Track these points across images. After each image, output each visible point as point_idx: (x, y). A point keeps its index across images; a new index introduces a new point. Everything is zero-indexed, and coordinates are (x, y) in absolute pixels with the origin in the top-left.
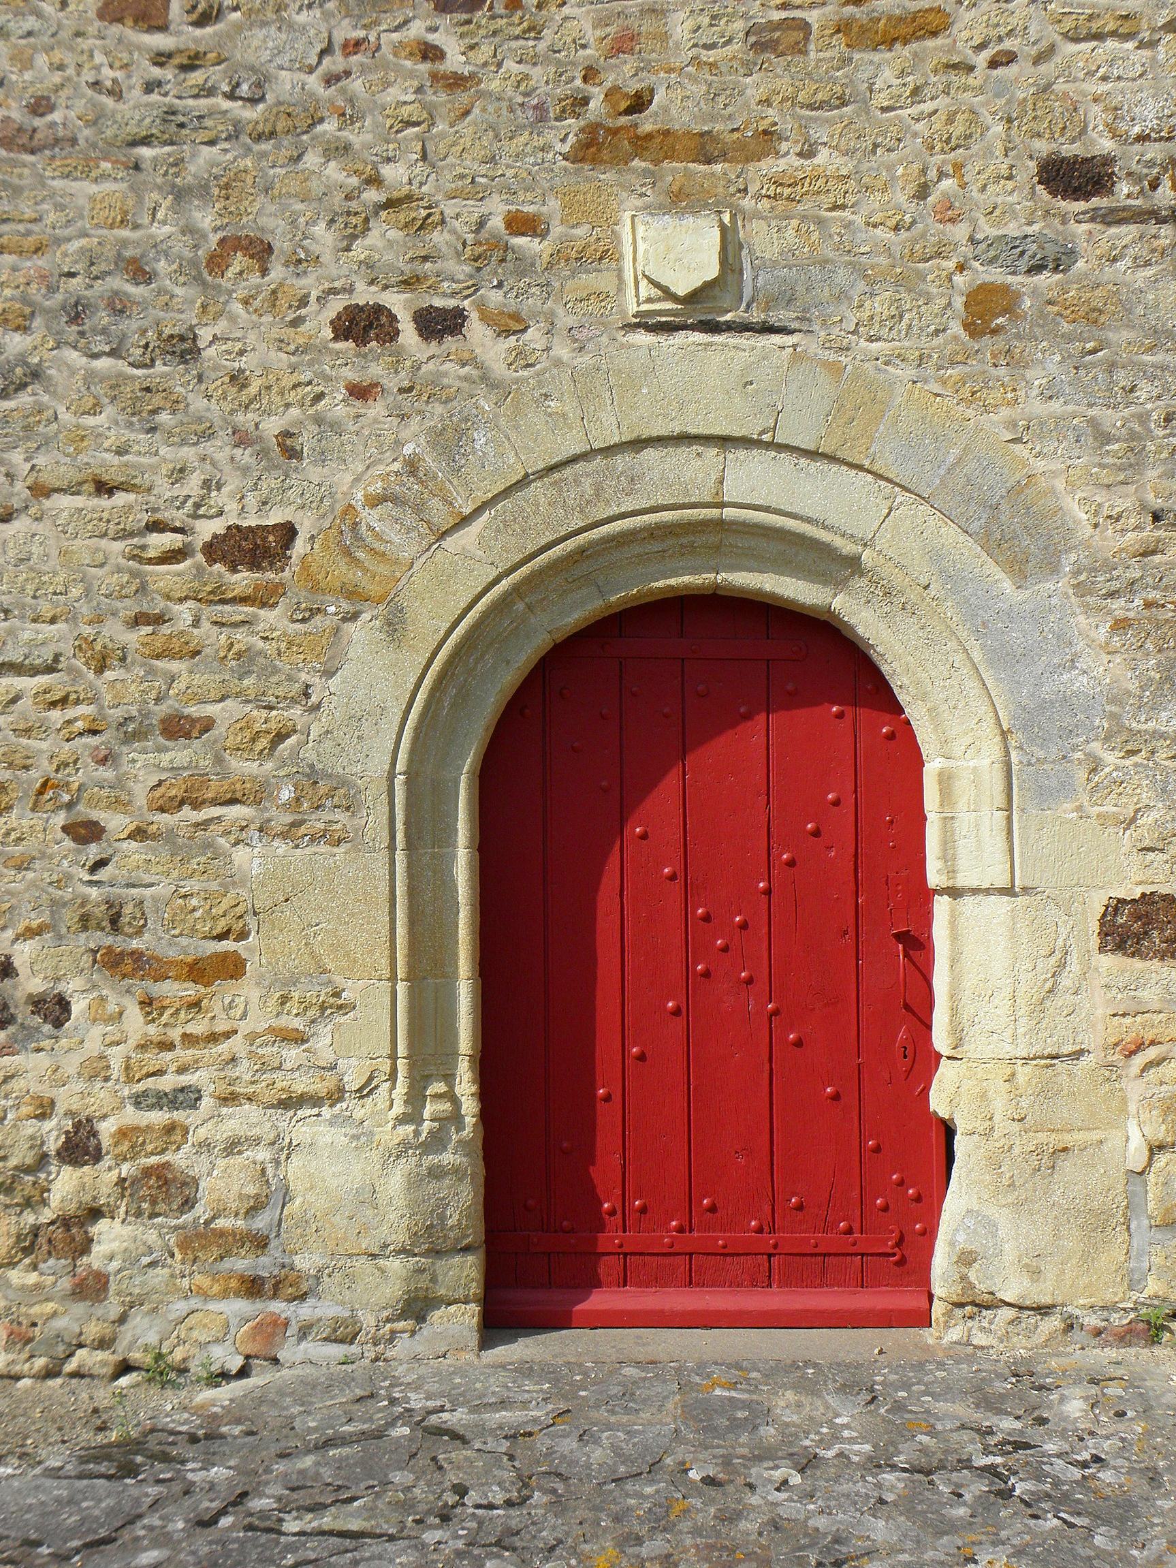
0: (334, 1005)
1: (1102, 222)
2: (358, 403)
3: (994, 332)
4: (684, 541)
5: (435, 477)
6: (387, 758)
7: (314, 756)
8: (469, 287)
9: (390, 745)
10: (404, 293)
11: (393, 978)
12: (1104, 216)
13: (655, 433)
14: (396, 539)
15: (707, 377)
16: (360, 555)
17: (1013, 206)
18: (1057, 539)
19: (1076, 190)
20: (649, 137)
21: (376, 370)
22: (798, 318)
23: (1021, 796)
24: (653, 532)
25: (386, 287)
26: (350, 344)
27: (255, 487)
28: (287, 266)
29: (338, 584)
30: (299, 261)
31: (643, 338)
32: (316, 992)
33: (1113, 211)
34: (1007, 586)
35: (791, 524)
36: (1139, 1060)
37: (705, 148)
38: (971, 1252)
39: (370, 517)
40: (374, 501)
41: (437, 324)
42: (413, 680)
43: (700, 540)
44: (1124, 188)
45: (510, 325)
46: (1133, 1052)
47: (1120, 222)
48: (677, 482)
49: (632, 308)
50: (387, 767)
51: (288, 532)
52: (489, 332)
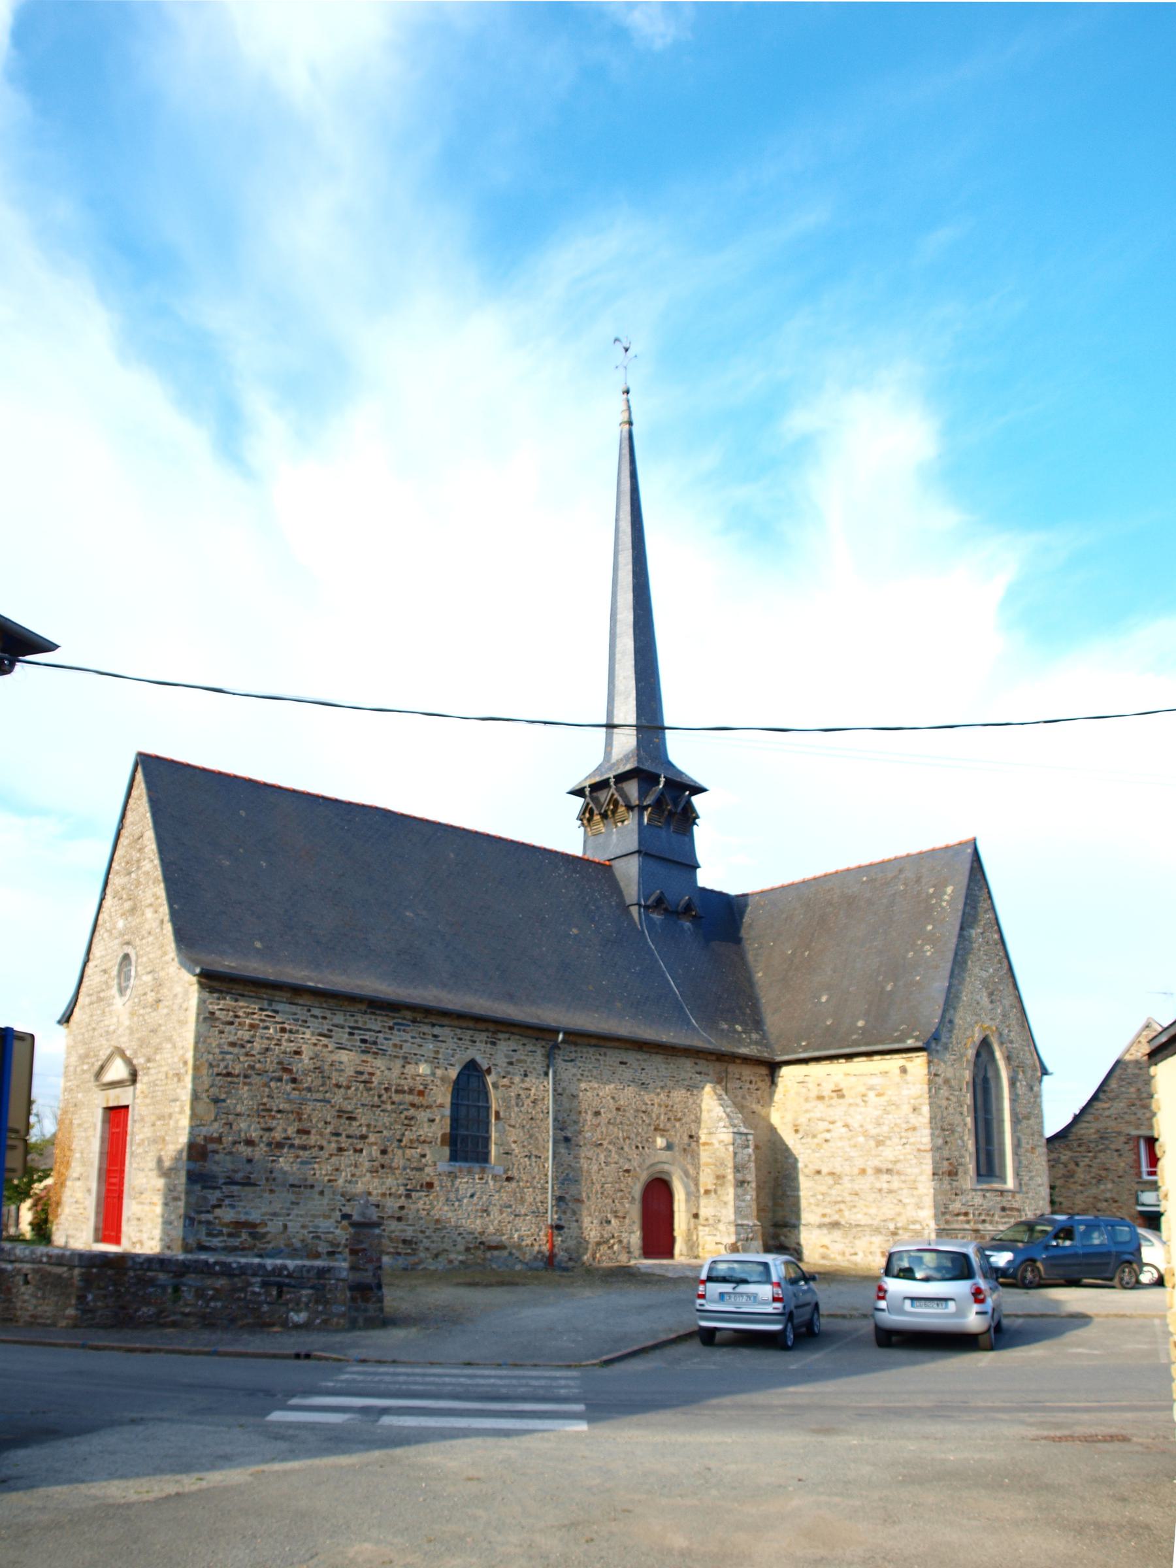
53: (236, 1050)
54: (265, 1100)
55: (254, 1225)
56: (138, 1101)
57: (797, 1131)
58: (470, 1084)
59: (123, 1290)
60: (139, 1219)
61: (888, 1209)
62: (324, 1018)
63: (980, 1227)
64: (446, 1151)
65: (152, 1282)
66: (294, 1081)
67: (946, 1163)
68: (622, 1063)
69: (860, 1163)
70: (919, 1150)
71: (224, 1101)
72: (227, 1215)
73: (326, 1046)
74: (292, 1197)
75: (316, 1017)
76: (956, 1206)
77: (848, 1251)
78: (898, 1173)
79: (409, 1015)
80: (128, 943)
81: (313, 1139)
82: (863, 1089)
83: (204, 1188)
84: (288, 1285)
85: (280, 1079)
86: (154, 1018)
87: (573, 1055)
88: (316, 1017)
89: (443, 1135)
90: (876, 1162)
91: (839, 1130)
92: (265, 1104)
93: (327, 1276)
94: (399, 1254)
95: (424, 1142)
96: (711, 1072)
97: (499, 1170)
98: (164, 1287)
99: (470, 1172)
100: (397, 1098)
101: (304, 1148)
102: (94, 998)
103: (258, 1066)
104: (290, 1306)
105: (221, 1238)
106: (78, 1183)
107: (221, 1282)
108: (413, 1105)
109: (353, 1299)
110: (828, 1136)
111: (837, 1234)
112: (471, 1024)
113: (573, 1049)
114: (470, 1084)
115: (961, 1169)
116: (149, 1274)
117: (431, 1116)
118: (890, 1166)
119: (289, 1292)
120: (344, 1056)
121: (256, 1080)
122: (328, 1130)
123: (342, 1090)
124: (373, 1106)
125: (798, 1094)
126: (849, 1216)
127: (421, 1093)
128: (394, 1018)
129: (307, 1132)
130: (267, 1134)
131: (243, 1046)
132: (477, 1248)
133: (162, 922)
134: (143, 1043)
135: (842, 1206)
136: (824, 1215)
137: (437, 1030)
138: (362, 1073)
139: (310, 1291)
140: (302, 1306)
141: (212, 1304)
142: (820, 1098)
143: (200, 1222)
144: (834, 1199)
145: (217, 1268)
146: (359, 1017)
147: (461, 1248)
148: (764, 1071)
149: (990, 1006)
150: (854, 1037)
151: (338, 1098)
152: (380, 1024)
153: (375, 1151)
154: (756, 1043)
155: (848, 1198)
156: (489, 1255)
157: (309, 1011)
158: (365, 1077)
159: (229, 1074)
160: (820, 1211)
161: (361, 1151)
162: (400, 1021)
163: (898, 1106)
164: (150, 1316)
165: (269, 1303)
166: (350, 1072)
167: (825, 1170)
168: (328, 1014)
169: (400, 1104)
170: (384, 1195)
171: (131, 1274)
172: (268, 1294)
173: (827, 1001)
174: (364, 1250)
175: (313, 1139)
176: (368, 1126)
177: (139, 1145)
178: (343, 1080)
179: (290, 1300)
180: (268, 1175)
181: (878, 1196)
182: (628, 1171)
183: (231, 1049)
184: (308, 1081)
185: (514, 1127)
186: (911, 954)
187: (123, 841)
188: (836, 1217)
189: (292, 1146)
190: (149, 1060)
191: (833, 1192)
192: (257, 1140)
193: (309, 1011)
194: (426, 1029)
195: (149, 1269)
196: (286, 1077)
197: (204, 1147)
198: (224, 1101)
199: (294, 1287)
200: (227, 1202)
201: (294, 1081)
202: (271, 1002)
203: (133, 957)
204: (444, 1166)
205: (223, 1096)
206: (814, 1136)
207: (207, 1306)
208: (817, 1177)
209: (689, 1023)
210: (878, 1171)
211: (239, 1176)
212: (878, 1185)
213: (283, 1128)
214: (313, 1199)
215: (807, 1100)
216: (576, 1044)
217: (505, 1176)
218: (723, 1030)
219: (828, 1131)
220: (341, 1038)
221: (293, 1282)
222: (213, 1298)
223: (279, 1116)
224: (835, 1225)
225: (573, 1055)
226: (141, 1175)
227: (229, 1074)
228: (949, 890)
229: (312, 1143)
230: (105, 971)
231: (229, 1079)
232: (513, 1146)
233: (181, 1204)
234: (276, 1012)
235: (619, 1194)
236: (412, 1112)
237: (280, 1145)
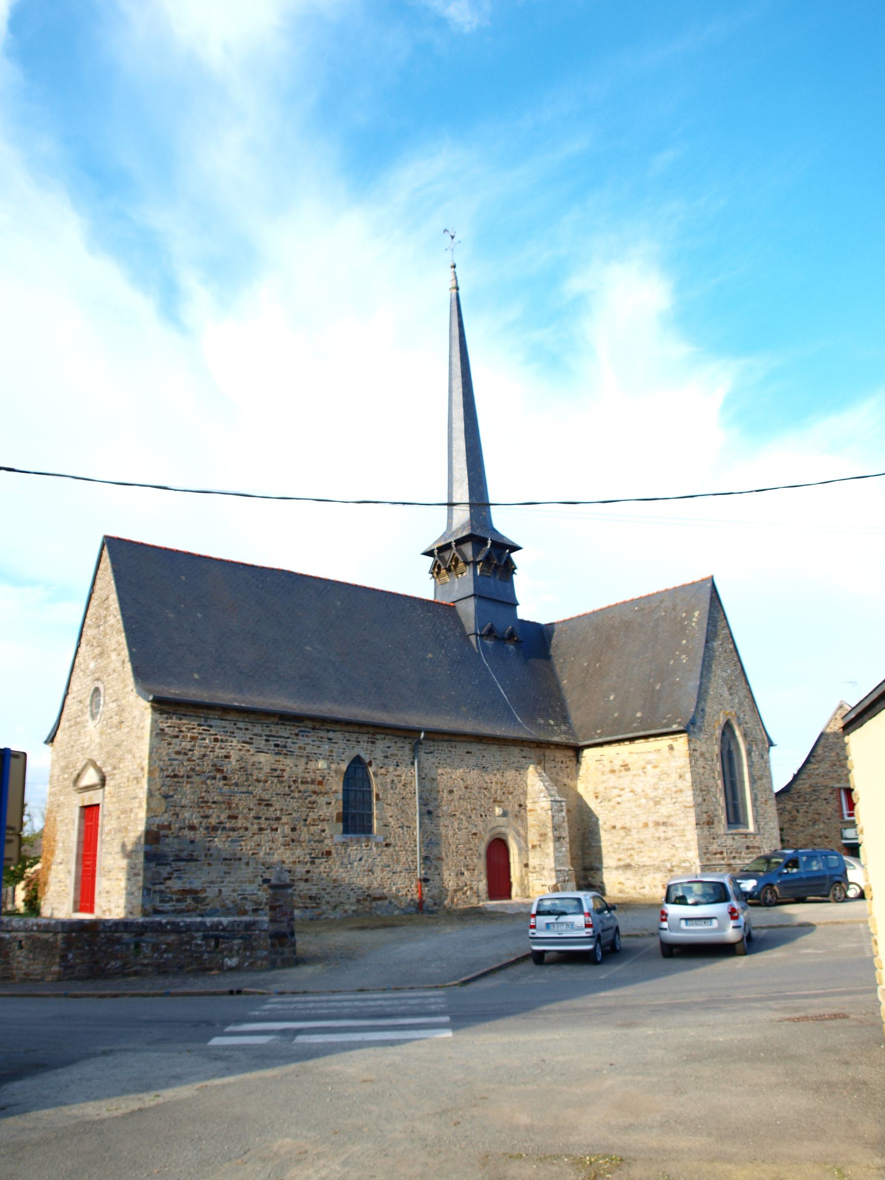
17: (517, 807)
53: (180, 757)
54: (203, 794)
55: (196, 892)
56: (106, 800)
57: (597, 797)
58: (357, 774)
59: (96, 948)
60: (108, 892)
61: (665, 852)
62: (247, 729)
63: (732, 862)
64: (340, 826)
65: (119, 941)
66: (225, 778)
67: (705, 815)
68: (468, 753)
69: (643, 819)
70: (685, 807)
71: (172, 796)
72: (176, 885)
73: (249, 751)
74: (225, 868)
75: (240, 729)
76: (714, 847)
77: (638, 886)
78: (672, 825)
79: (310, 724)
80: (98, 679)
81: (240, 822)
82: (642, 763)
83: (158, 865)
84: (223, 937)
85: (214, 778)
86: (119, 735)
87: (432, 749)
88: (240, 729)
89: (338, 814)
90: (655, 818)
91: (627, 795)
92: (203, 798)
93: (253, 928)
94: (306, 908)
95: (324, 820)
96: (533, 756)
97: (380, 839)
98: (128, 945)
99: (358, 841)
100: (302, 787)
101: (233, 829)
102: (72, 722)
103: (197, 768)
104: (225, 953)
105: (171, 904)
106: (61, 867)
107: (172, 938)
108: (315, 792)
109: (273, 945)
110: (619, 799)
111: (629, 873)
112: (356, 729)
113: (432, 743)
114: (357, 774)
115: (716, 820)
116: (117, 935)
117: (329, 800)
118: (665, 820)
119: (224, 943)
120: (262, 758)
121: (196, 779)
122: (251, 815)
123: (261, 784)
124: (284, 795)
125: (596, 769)
126: (638, 859)
127: (320, 783)
128: (299, 727)
129: (236, 818)
130: (205, 821)
131: (186, 754)
132: (365, 900)
133: (124, 662)
134: (110, 755)
135: (632, 852)
136: (619, 860)
137: (331, 735)
138: (275, 770)
139: (240, 941)
140: (234, 953)
141: (165, 956)
142: (613, 771)
143: (155, 892)
144: (626, 847)
145: (169, 927)
146: (273, 727)
147: (353, 900)
148: (571, 753)
149: (730, 698)
150: (635, 725)
151: (258, 790)
152: (288, 732)
153: (287, 829)
154: (565, 733)
155: (636, 846)
156: (374, 904)
157: (235, 724)
158: (278, 773)
159: (175, 776)
160: (616, 856)
161: (276, 829)
162: (303, 729)
163: (668, 775)
164: (117, 968)
165: (209, 952)
166: (267, 769)
167: (618, 826)
168: (250, 726)
169: (305, 792)
170: (294, 862)
171: (102, 935)
172: (208, 945)
173: (614, 699)
174: (280, 906)
175: (240, 822)
176: (281, 810)
177: (108, 834)
178: (262, 776)
179: (225, 949)
180: (206, 852)
181: (657, 843)
182: (475, 834)
183: (177, 757)
184: (235, 778)
185: (390, 805)
186: (672, 662)
187: (94, 602)
188: (628, 861)
189: (224, 829)
190: (114, 768)
191: (626, 842)
192: (197, 825)
193: (235, 724)
194: (323, 734)
195: (116, 931)
196: (219, 776)
197: (157, 833)
198: (172, 796)
199: (228, 938)
200: (175, 875)
201: (225, 778)
202: (206, 719)
203: (102, 690)
204: (339, 838)
205: (171, 793)
206: (610, 801)
207: (161, 957)
208: (613, 831)
209: (516, 720)
210: (657, 824)
211: (184, 854)
212: (657, 835)
213: (218, 815)
214: (241, 869)
215: (603, 773)
216: (434, 740)
217: (384, 843)
218: (540, 724)
219: (619, 796)
220: (260, 744)
221: (227, 935)
222: (166, 951)
223: (214, 806)
224: (628, 866)
225: (432, 749)
226: (109, 857)
227: (175, 776)
228: (696, 614)
229: (239, 825)
230: (80, 702)
231: (176, 780)
232: (390, 819)
233: (141, 878)
234: (211, 726)
235: (470, 852)
236: (314, 798)
237: (215, 829)
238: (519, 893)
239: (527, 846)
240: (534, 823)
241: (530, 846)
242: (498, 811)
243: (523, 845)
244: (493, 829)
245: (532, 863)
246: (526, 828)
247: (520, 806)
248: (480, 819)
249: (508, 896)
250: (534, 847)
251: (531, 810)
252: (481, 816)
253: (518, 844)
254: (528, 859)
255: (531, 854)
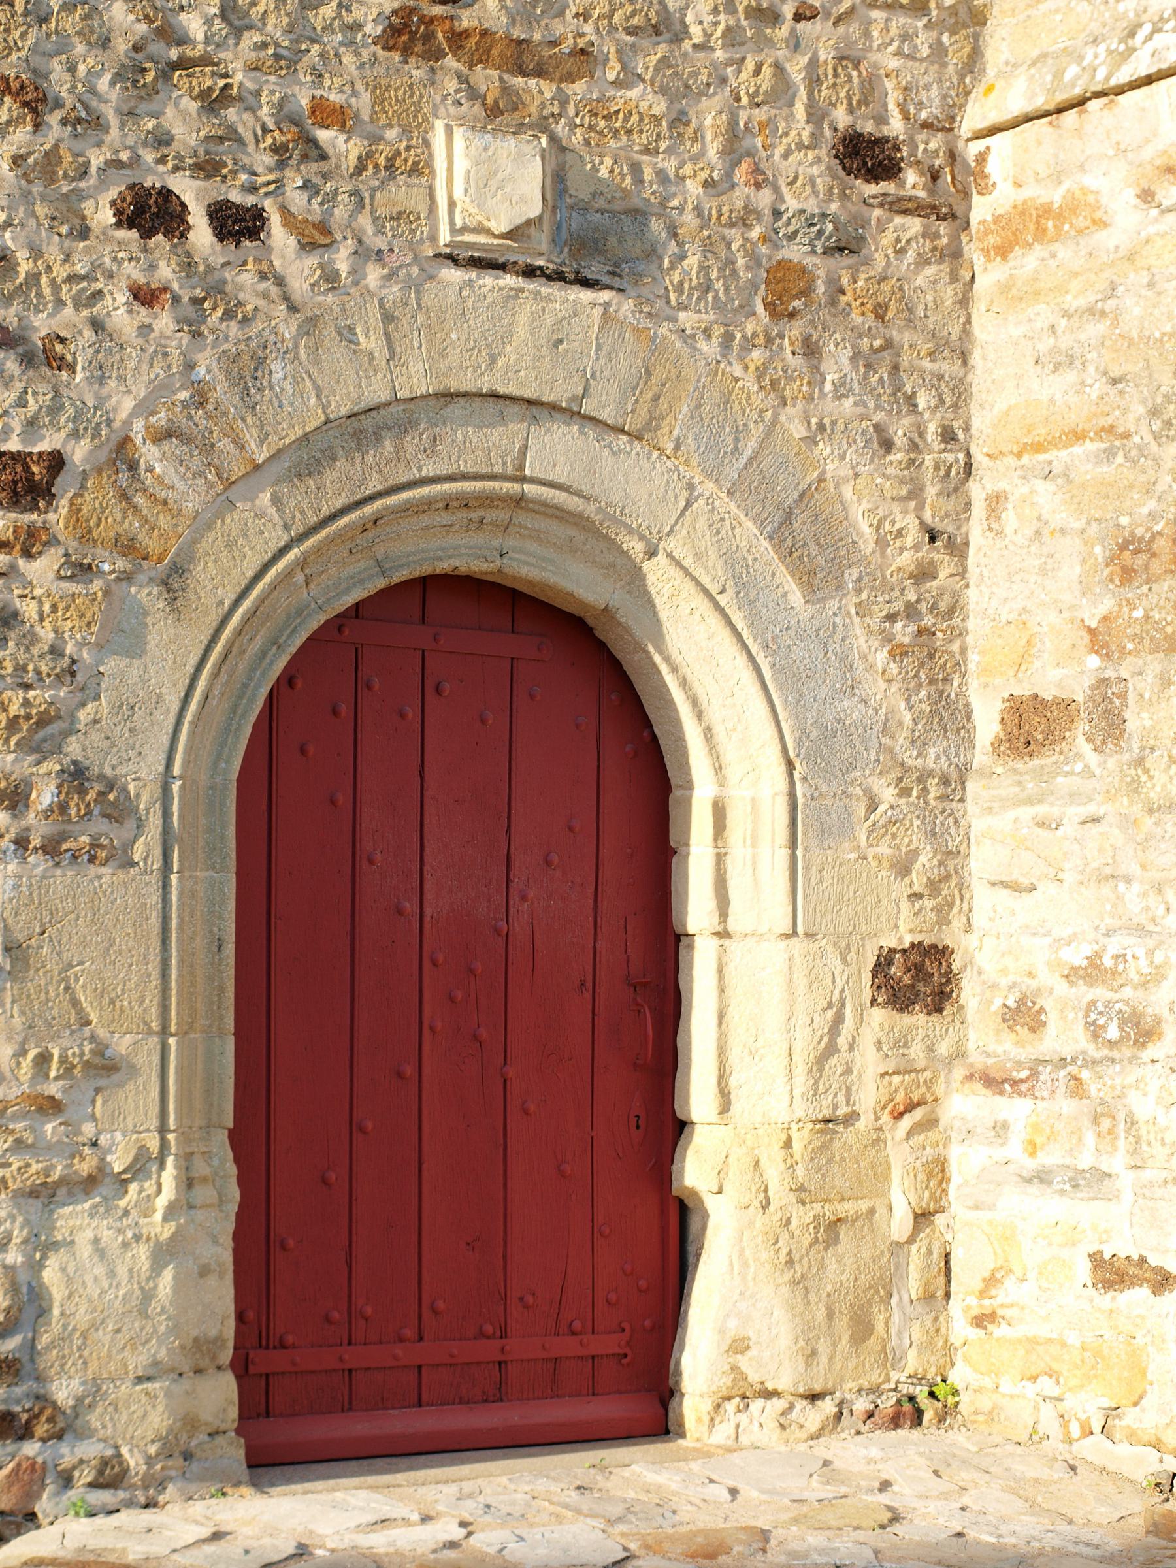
0: (104, 1067)
1: (890, 210)
2: (143, 311)
3: (792, 315)
4: (474, 515)
5: (226, 414)
6: (163, 757)
7: (78, 751)
8: (269, 183)
9: (165, 740)
10: (198, 178)
11: (164, 1031)
12: (891, 203)
13: (463, 388)
14: (180, 485)
15: (537, 332)
16: (139, 500)
17: (804, 176)
18: (842, 552)
19: (869, 171)
20: (465, 34)
21: (166, 272)
22: (609, 273)
23: (805, 833)
24: (465, 502)
25: (176, 169)
26: (134, 234)
27: (21, 403)
28: (65, 124)
29: (112, 534)
30: (79, 121)
31: (452, 275)
32: (78, 1049)
33: (900, 199)
34: (796, 597)
35: (559, 497)
36: (907, 1122)
37: (522, 58)
38: (743, 1340)
39: (149, 454)
40: (160, 436)
41: (234, 223)
42: (193, 660)
43: (490, 515)
44: (911, 177)
45: (315, 237)
46: (901, 1114)
47: (906, 212)
48: (475, 449)
49: (445, 236)
50: (161, 768)
51: (56, 462)
52: (292, 241)
238: (778, 1364)
239: (947, 715)
240: (1054, 389)
241: (987, 723)
242: (481, 179)
243: (882, 687)
244: (363, 427)
245: (994, 950)
246: (939, 464)
247: (865, 156)
248: (127, 257)
249: (647, 1407)
250: (1033, 727)
251: (1034, 224)
252: (152, 214)
253: (790, 673)
254: (945, 887)
255: (997, 821)
